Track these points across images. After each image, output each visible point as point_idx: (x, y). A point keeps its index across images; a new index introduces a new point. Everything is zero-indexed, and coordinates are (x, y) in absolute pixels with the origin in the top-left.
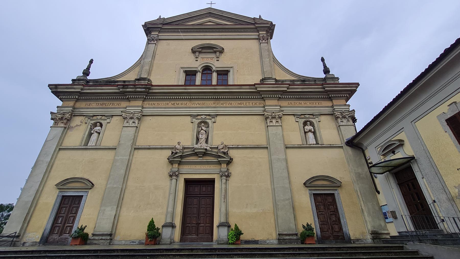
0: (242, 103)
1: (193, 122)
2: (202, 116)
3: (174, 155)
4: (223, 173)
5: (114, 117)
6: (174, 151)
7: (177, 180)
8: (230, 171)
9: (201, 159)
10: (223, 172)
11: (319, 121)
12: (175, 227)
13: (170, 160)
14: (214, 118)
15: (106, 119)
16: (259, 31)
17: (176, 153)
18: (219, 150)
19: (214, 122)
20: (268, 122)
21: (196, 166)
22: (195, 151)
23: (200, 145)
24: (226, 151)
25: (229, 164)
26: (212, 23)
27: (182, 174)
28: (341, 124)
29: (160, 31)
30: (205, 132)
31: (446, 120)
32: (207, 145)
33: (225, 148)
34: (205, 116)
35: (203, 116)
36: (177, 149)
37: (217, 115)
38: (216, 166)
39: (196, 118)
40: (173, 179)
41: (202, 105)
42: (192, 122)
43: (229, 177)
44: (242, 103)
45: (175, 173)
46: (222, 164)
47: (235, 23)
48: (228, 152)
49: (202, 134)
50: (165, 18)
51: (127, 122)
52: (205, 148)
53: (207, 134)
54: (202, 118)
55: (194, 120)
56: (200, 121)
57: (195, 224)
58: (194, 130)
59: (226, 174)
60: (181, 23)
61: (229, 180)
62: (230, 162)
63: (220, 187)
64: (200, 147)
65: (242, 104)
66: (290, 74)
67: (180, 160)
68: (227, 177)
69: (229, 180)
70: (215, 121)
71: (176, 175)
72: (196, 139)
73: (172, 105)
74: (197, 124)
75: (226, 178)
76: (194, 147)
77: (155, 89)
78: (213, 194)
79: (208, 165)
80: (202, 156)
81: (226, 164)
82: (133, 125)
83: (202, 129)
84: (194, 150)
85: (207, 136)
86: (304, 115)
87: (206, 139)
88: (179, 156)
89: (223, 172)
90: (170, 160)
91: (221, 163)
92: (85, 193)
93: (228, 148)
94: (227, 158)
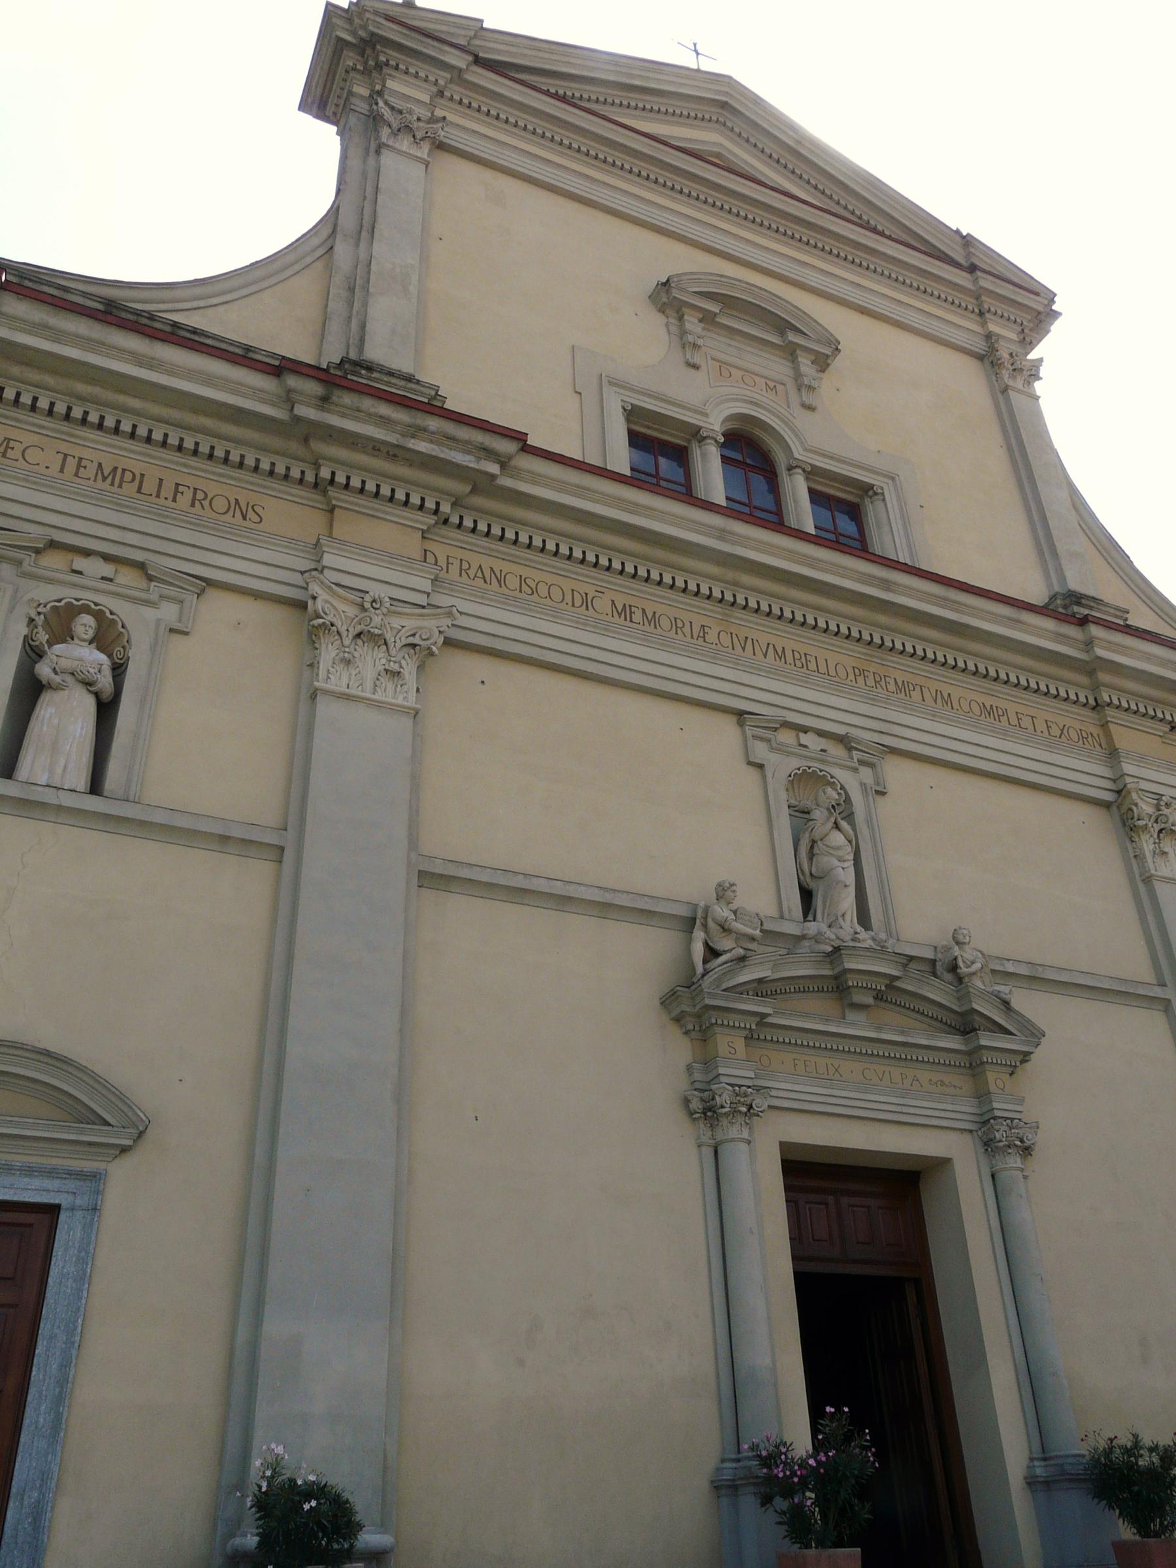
0: (128, 476)
2: (805, 739)
5: (212, 594)
11: (878, 788)
15: (154, 597)
16: (988, 315)
20: (324, 665)
26: (813, 198)
28: (339, 680)
29: (441, 94)
34: (823, 743)
35: (810, 735)
37: (210, 583)
41: (799, 664)
44: (128, 476)
47: (828, 201)
50: (485, 25)
51: (348, 662)
55: (761, 752)
56: (793, 764)
60: (597, 101)
65: (122, 481)
66: (1147, 601)
73: (104, 479)
77: (535, 479)
82: (388, 693)
86: (793, 733)
88: (747, 987)
92: (72, 1185)
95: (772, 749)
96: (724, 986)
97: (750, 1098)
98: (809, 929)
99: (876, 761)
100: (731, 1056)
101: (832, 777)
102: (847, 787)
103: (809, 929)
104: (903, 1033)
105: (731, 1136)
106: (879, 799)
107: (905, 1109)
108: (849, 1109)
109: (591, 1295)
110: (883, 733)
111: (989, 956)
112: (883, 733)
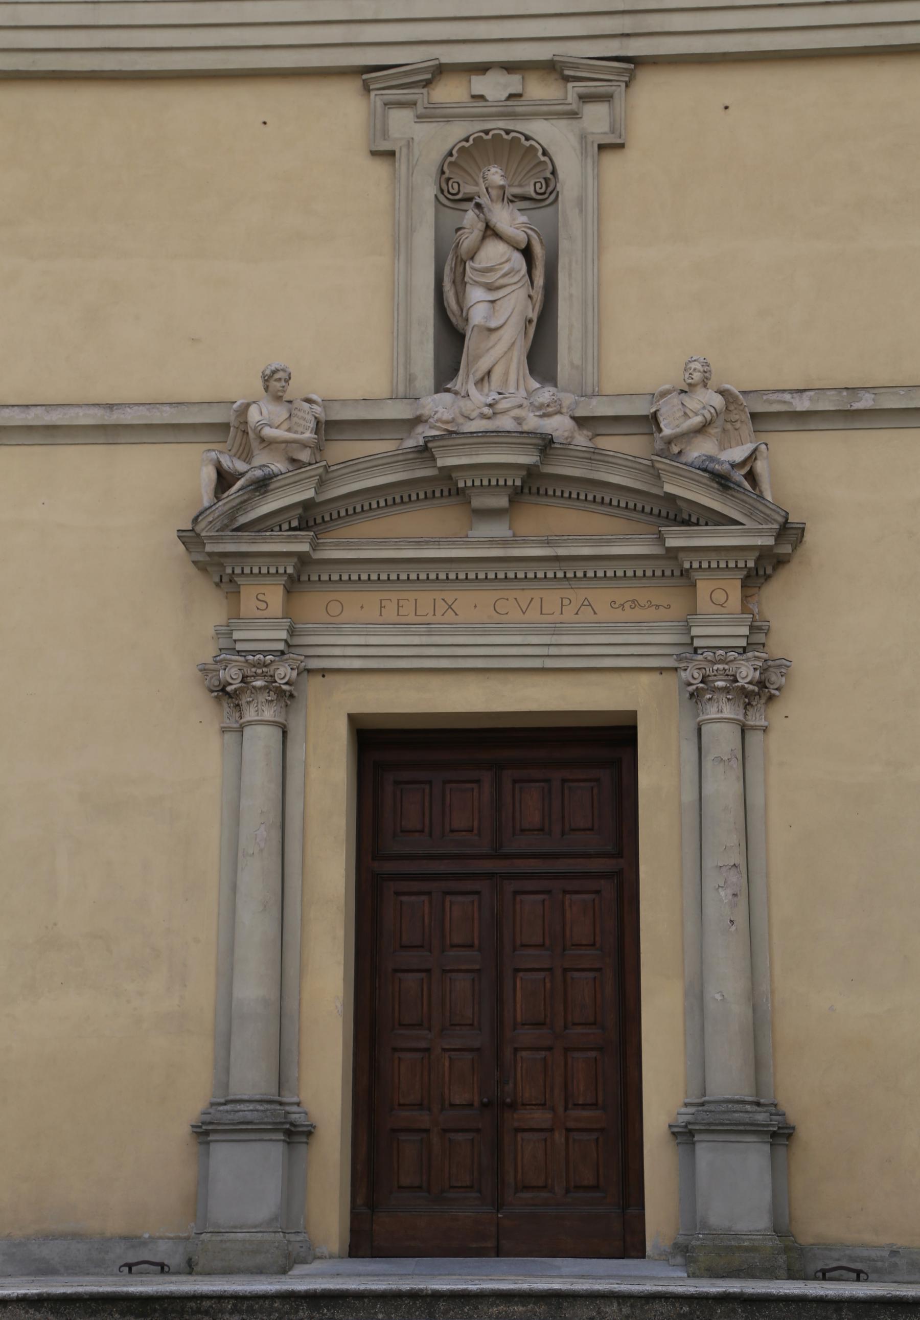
1: (391, 154)
2: (481, 84)
3: (241, 507)
4: (250, 671)
6: (241, 466)
7: (285, 733)
8: (776, 647)
9: (500, 529)
10: (709, 655)
12: (309, 1134)
13: (209, 548)
14: (607, 98)
17: (262, 485)
18: (669, 441)
19: (601, 147)
21: (450, 596)
22: (440, 463)
23: (479, 398)
24: (738, 454)
25: (767, 577)
27: (324, 672)
30: (518, 260)
31: (635, 712)
32: (546, 395)
33: (722, 417)
34: (513, 83)
36: (262, 440)
37: (636, 62)
38: (643, 595)
39: (420, 110)
40: (250, 723)
42: (385, 146)
43: (771, 698)
45: (264, 675)
46: (700, 584)
48: (761, 467)
49: (490, 288)
52: (532, 422)
53: (539, 280)
54: (479, 108)
56: (456, 132)
57: (470, 1105)
58: (410, 231)
59: (746, 673)
61: (765, 730)
62: (777, 556)
63: (689, 796)
64: (483, 416)
67: (305, 547)
68: (747, 706)
69: (765, 730)
70: (613, 131)
71: (280, 693)
72: (431, 331)
74: (434, 170)
75: (741, 717)
76: (418, 420)
78: (620, 855)
79: (569, 593)
80: (503, 502)
81: (738, 583)
83: (490, 232)
84: (425, 451)
85: (538, 296)
87: (532, 330)
89: (709, 655)
90: (210, 554)
91: (685, 574)
93: (754, 416)
94: (749, 524)
95: (420, 118)
96: (243, 520)
97: (272, 668)
98: (424, 407)
99: (416, 97)
100: (259, 614)
101: (528, 138)
102: (551, 150)
103: (424, 407)
104: (548, 543)
105: (248, 718)
106: (611, 160)
107: (553, 651)
108: (460, 660)
109: (55, 924)
110: (628, 35)
111: (744, 393)
112: (628, 35)
